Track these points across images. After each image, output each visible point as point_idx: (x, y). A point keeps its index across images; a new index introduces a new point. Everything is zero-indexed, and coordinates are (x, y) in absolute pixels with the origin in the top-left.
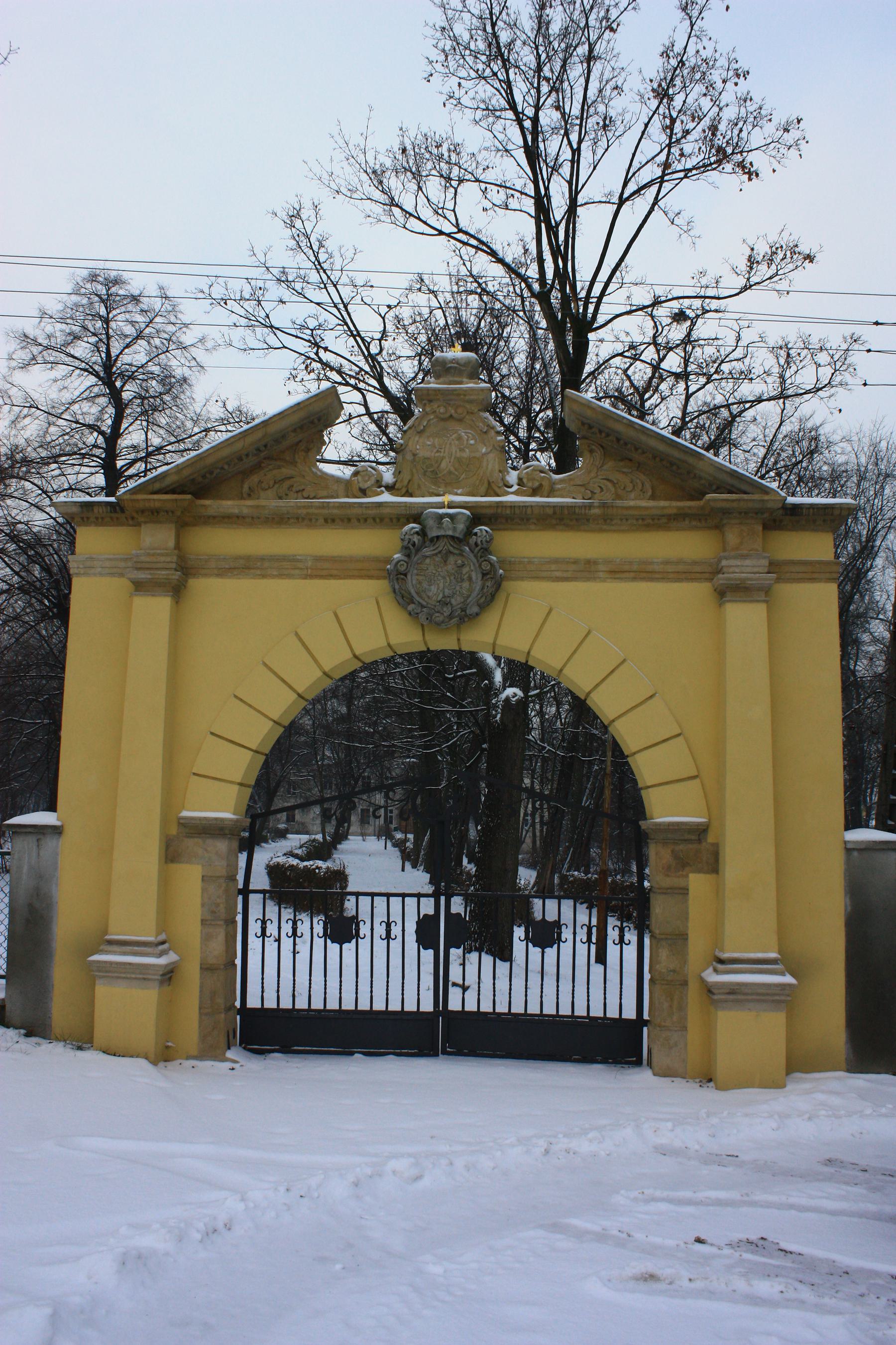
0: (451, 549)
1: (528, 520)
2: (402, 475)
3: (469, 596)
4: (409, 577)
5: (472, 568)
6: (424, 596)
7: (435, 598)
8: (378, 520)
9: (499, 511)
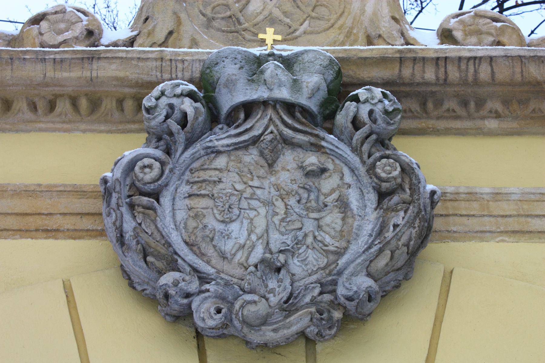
0: (288, 132)
1: (480, 103)
2: (150, 25)
3: (339, 253)
4: (166, 199)
5: (348, 178)
6: (210, 252)
7: (240, 257)
8: (84, 103)
9: (407, 72)
